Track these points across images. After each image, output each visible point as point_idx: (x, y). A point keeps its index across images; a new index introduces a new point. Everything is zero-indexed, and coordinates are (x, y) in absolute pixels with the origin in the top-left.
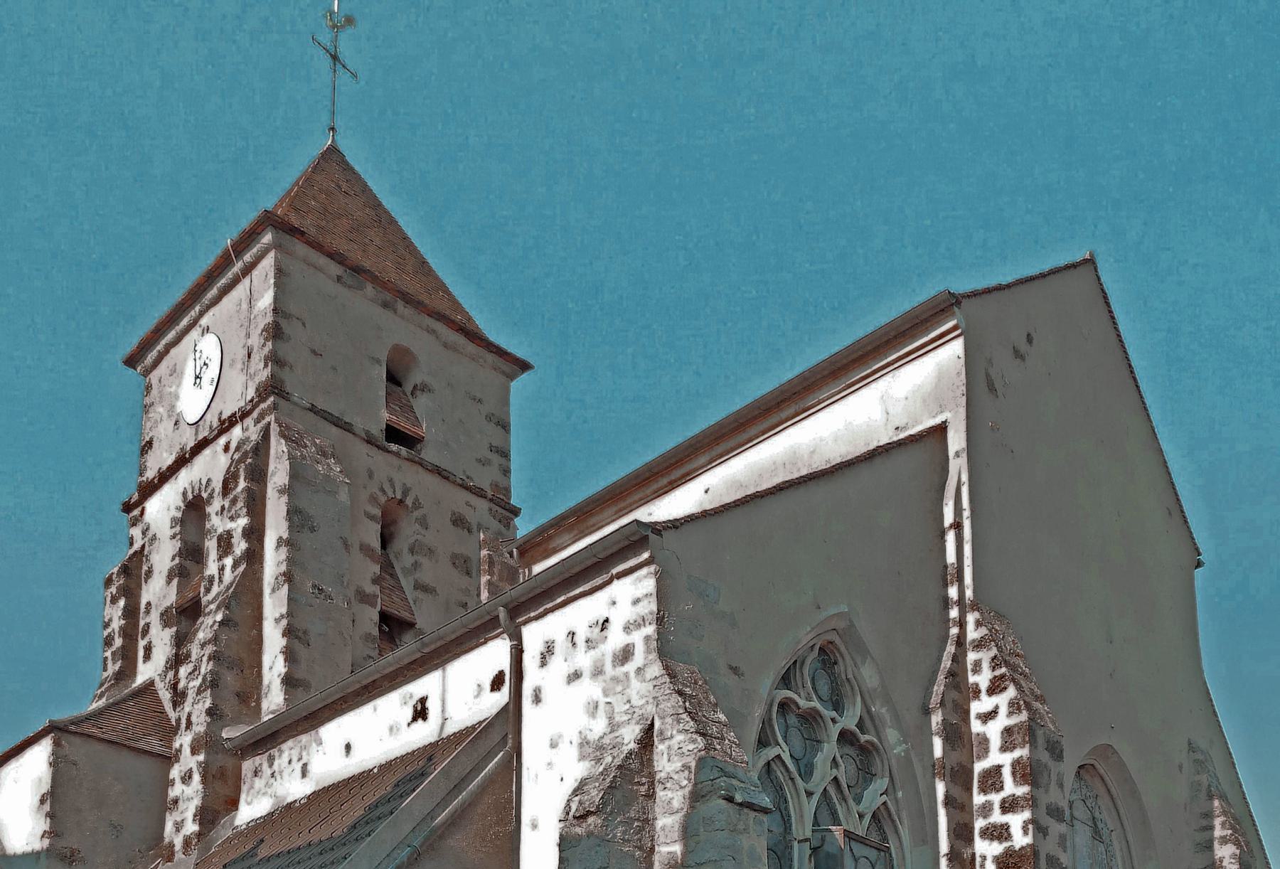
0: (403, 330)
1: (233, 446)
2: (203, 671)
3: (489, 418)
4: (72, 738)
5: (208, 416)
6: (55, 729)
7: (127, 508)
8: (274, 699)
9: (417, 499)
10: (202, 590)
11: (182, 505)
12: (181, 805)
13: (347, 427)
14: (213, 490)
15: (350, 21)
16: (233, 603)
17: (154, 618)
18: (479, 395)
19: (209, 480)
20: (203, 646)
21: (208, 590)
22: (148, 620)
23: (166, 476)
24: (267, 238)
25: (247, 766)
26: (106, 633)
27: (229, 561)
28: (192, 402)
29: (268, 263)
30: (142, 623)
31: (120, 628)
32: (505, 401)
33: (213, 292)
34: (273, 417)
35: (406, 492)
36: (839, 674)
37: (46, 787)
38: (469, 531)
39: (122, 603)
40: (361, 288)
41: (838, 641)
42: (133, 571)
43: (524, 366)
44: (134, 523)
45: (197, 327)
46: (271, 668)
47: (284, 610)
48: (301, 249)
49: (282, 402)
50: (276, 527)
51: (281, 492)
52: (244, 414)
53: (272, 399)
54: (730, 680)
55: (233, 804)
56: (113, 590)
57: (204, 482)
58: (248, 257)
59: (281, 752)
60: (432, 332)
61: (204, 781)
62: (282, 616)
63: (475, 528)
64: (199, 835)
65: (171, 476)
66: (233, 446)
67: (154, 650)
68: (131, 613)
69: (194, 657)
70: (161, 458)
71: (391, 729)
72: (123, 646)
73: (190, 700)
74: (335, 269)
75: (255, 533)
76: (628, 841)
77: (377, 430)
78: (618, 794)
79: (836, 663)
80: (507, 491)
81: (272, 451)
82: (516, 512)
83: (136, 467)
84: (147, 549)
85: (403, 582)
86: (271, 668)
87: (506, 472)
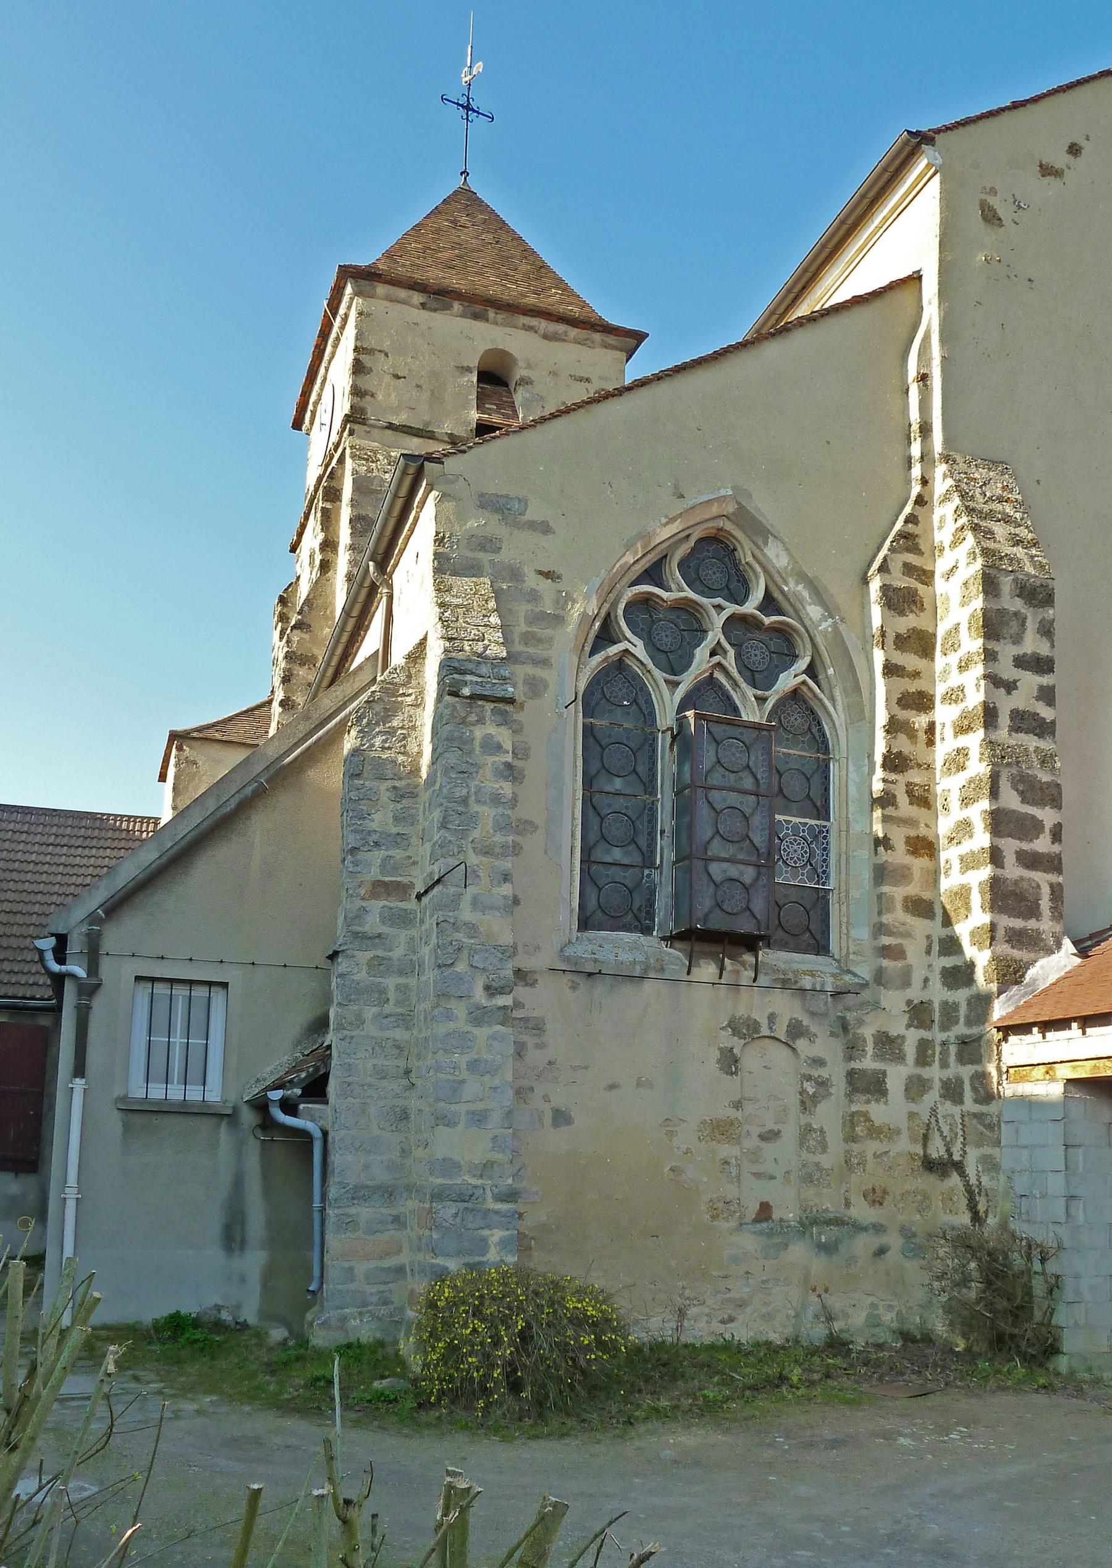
4: (192, 742)
18: (585, 375)
24: (349, 290)
33: (329, 349)
36: (740, 560)
40: (448, 307)
41: (729, 526)
49: (356, 427)
54: (545, 586)
60: (530, 328)
74: (417, 298)
76: (389, 748)
78: (378, 708)
79: (735, 550)
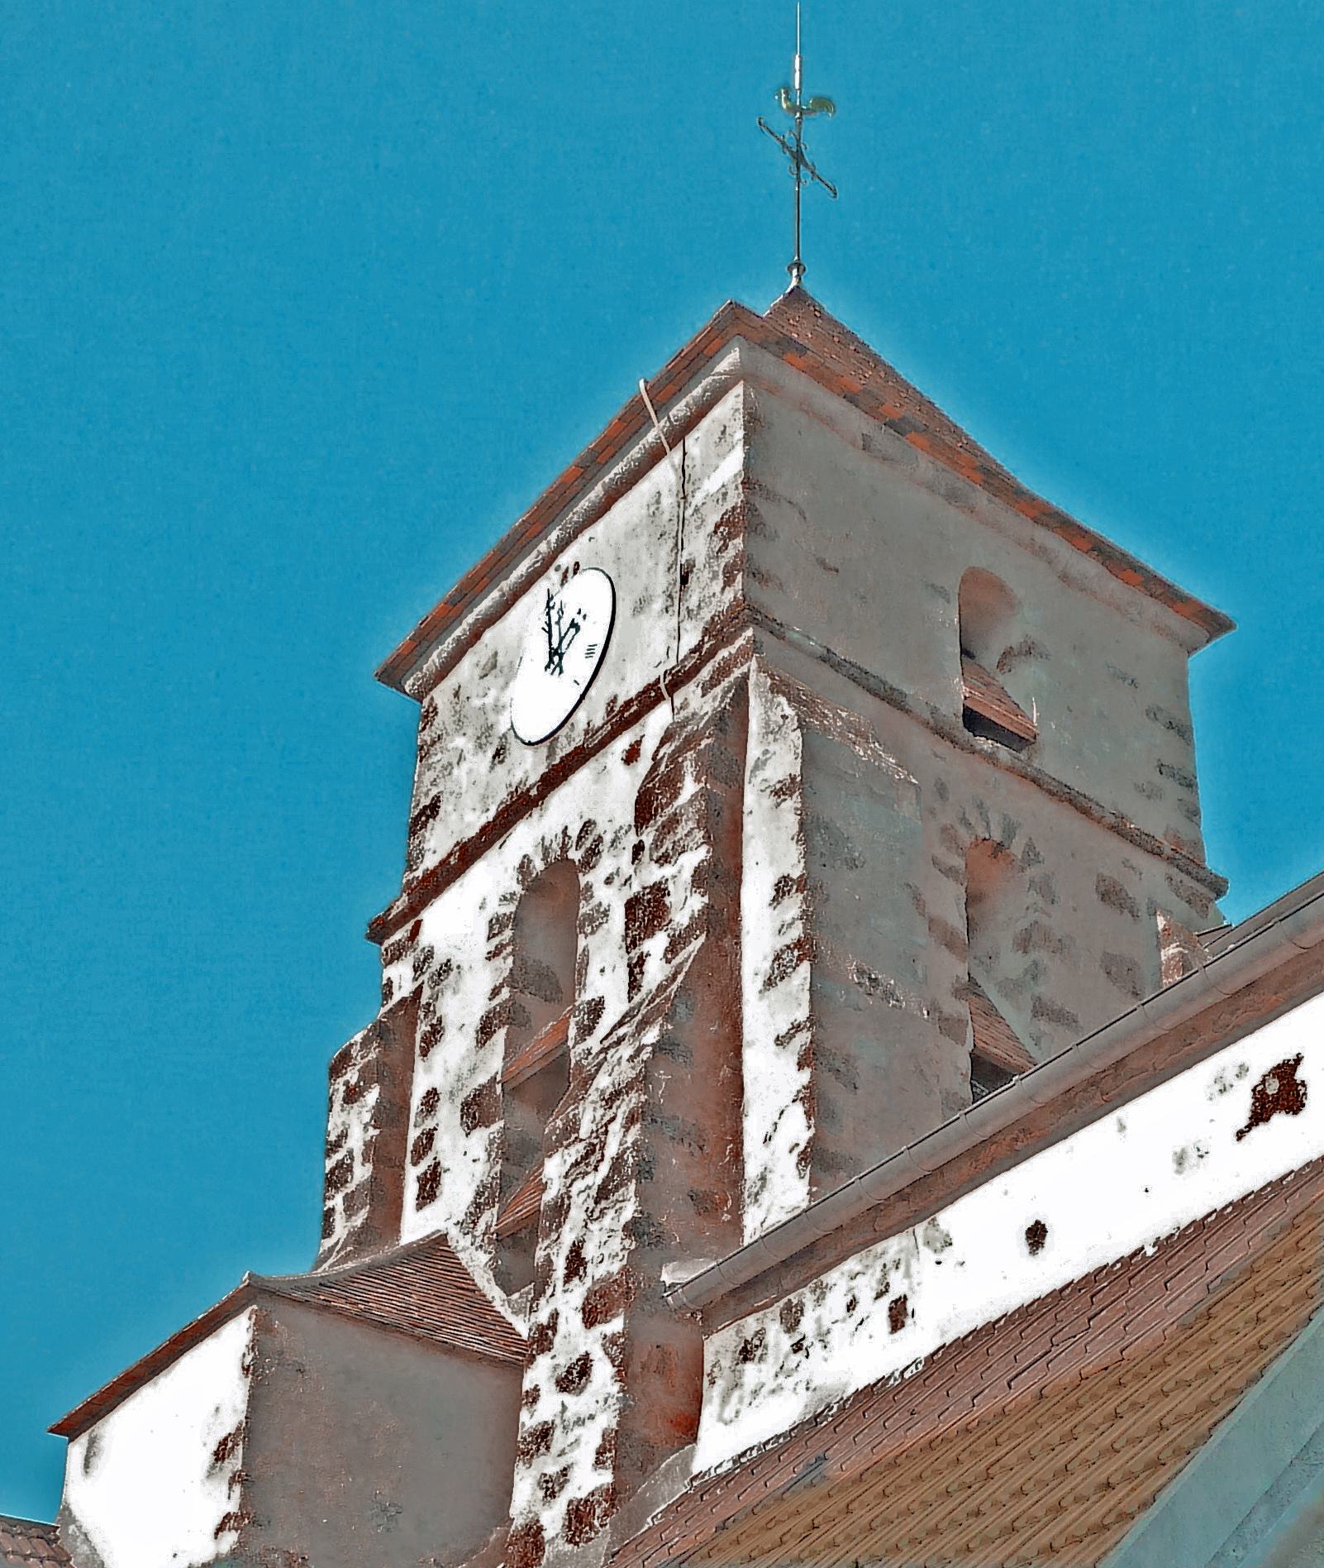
0: (990, 544)
1: (648, 748)
2: (612, 1150)
3: (1153, 714)
5: (581, 717)
6: (256, 1293)
7: (380, 930)
8: (779, 1193)
9: (1030, 846)
10: (572, 1032)
11: (518, 889)
12: (559, 1440)
13: (893, 699)
14: (600, 839)
15: (823, 103)
16: (681, 1009)
17: (447, 1115)
19: (588, 826)
20: (611, 1100)
21: (586, 1030)
22: (429, 1124)
23: (468, 853)
24: (729, 361)
25: (719, 1346)
26: (330, 1164)
27: (656, 945)
28: (537, 703)
29: (734, 399)
30: (413, 1134)
31: (367, 1145)
32: (1180, 688)
33: (597, 492)
34: (753, 664)
35: (1010, 830)
37: (230, 1422)
38: (1135, 916)
39: (372, 1096)
42: (408, 1028)
43: (1216, 624)
44: (396, 955)
45: (551, 572)
46: (767, 1139)
47: (802, 1014)
48: (798, 383)
49: (767, 639)
50: (769, 850)
51: (781, 792)
52: (677, 679)
53: (749, 633)
55: (688, 1429)
56: (352, 1076)
57: (574, 832)
58: (679, 410)
59: (821, 1293)
60: (1041, 552)
61: (623, 1372)
62: (797, 1028)
63: (1143, 913)
64: (612, 1495)
65: (488, 845)
66: (648, 748)
67: (446, 1179)
68: (391, 1115)
69: (585, 1129)
70: (462, 820)
71: (1180, 1159)
72: (374, 1179)
73: (576, 1215)
75: (722, 878)
77: (952, 710)
80: (1197, 844)
81: (754, 726)
82: (1218, 888)
83: (402, 853)
84: (426, 993)
85: (1004, 1007)
86: (767, 1139)
87: (1193, 813)
